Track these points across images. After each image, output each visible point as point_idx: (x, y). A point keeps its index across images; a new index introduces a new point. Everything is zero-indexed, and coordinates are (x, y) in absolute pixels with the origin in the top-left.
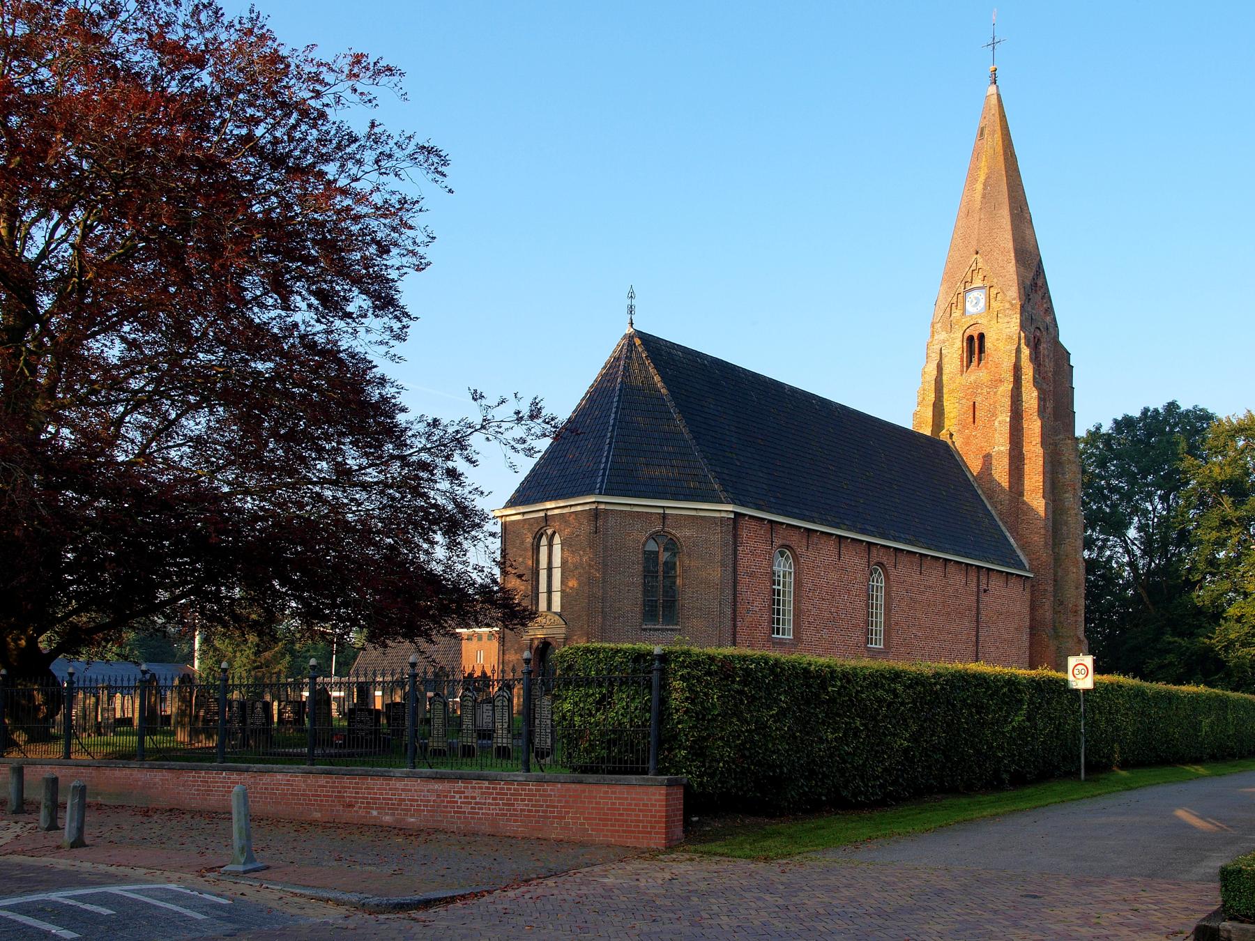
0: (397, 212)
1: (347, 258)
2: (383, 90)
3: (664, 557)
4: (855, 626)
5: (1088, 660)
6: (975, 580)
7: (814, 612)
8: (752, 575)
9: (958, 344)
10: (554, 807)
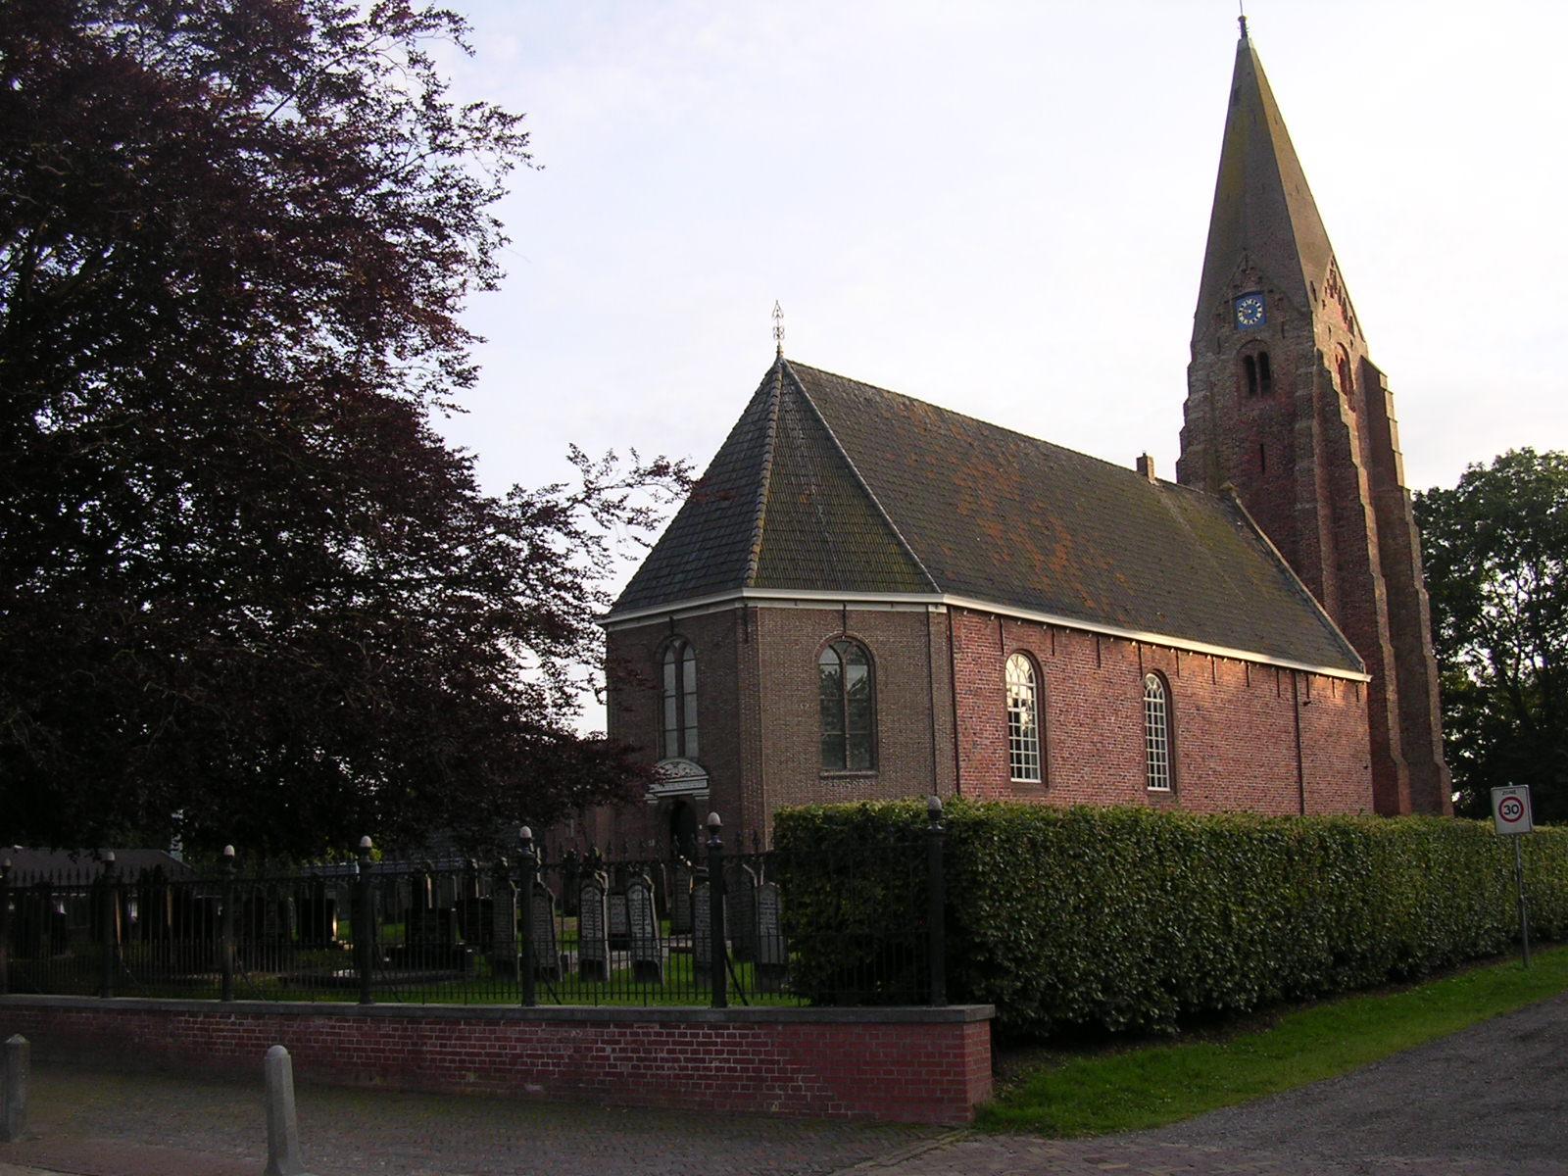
0: (461, 203)
1: (389, 265)
2: (435, 44)
3: (855, 674)
4: (1131, 760)
5: (1522, 793)
6: (1304, 684)
7: (1069, 742)
8: (977, 693)
9: (1231, 368)
10: (772, 1062)
